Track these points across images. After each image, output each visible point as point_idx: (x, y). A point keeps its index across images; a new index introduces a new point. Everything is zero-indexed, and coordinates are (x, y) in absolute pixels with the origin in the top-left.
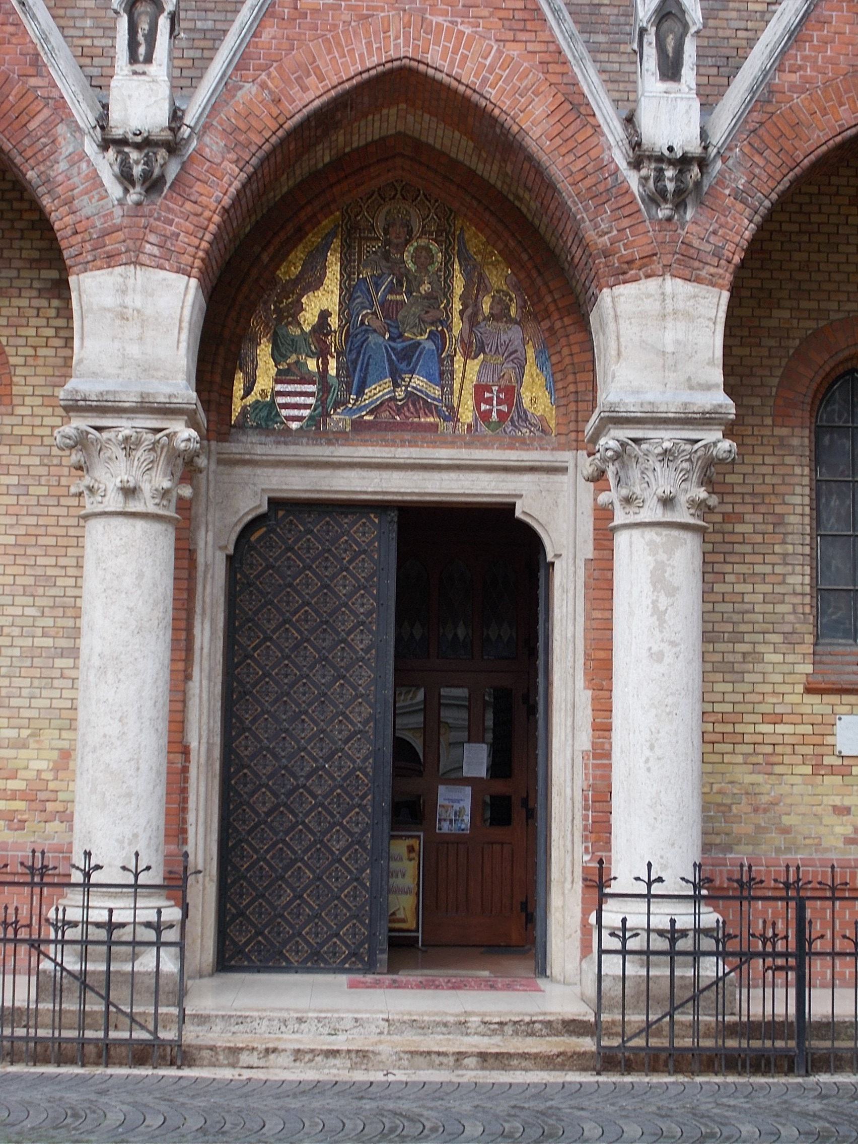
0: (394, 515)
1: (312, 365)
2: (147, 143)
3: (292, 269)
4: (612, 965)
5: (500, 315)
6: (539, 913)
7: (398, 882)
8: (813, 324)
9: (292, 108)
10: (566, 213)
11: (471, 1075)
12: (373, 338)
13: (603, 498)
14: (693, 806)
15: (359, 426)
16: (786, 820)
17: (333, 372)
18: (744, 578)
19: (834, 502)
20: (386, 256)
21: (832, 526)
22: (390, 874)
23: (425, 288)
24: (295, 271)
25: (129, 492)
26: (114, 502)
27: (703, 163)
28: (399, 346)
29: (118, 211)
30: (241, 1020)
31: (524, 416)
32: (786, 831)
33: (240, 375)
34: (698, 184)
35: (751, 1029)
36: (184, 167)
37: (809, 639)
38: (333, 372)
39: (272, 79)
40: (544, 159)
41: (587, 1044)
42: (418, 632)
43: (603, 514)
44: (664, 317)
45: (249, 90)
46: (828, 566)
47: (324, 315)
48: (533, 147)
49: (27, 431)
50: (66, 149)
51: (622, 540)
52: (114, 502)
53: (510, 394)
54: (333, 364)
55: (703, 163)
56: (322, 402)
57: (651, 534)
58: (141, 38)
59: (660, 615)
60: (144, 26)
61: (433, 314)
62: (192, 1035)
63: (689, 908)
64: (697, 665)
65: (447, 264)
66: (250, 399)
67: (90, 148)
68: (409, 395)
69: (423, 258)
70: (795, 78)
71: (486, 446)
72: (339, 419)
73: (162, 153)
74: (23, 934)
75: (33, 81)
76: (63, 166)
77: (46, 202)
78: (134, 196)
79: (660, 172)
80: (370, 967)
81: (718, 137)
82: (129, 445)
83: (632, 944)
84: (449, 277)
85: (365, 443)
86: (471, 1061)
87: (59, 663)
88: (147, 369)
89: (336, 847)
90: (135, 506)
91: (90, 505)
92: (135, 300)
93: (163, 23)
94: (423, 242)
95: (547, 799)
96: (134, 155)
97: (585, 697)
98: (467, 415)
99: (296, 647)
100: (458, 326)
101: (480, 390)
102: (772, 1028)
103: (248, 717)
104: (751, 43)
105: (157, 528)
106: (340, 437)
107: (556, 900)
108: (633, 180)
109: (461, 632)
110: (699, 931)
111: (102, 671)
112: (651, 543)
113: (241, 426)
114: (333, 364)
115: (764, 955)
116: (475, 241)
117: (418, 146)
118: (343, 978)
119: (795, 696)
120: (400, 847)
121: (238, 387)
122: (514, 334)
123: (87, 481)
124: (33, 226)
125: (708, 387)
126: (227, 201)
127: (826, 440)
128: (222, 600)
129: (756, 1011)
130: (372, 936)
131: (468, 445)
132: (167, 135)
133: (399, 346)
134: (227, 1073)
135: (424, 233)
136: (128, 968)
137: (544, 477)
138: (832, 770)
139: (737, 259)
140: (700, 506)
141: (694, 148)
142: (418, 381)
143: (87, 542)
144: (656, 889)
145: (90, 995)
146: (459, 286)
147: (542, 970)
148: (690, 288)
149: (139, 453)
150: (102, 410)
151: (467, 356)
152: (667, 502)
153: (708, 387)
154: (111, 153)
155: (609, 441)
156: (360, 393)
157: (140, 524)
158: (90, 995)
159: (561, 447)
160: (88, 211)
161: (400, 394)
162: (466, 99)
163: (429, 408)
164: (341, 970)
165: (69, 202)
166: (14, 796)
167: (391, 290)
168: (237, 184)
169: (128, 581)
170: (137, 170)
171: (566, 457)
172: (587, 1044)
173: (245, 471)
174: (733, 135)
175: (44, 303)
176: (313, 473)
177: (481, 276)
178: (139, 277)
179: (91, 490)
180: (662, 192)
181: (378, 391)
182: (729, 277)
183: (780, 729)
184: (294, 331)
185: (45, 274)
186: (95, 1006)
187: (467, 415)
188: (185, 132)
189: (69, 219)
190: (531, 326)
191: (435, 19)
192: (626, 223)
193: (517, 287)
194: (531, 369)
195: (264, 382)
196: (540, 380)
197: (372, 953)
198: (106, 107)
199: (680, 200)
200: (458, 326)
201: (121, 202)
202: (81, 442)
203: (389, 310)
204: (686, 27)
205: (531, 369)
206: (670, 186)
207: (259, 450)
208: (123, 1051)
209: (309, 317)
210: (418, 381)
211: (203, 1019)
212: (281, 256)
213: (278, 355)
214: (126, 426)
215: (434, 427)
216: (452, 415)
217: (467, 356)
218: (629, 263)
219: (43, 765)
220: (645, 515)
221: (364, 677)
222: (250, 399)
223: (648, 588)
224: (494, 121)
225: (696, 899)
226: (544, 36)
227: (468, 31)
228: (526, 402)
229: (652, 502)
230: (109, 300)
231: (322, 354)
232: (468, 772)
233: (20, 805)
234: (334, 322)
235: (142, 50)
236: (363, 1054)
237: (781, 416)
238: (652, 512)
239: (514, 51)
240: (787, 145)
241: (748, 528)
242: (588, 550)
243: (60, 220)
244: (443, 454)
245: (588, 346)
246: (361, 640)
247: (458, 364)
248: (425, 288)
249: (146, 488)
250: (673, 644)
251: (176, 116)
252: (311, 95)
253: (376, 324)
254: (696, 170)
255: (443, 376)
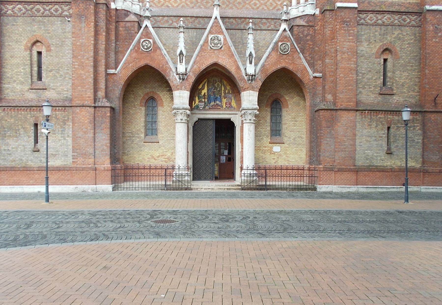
0: (215, 120)
1: (203, 100)
2: (183, 74)
3: (200, 87)
4: (243, 178)
5: (229, 93)
6: (234, 159)
7: (215, 169)
8: (271, 94)
9: (201, 69)
10: (237, 82)
11: (226, 191)
12: (211, 96)
13: (242, 119)
14: (253, 158)
15: (210, 108)
16: (267, 160)
17: (206, 101)
18: (261, 128)
19: (274, 118)
20: (213, 85)
21: (273, 121)
22: (215, 168)
23: (218, 89)
24: (201, 87)
25: (181, 120)
26: (180, 121)
27: (255, 76)
28: (215, 97)
29: (179, 83)
30: (198, 185)
31: (232, 107)
32: (266, 161)
33: (194, 102)
34: (254, 78)
35: (260, 185)
36: (187, 77)
37: (270, 136)
38: (206, 101)
39: (198, 65)
40: (234, 75)
41: (240, 187)
42: (217, 135)
43: (242, 121)
44: (250, 96)
45: (195, 66)
46: (273, 126)
47: (205, 93)
48: (233, 73)
49: (166, 110)
50: (172, 75)
51: (244, 124)
52: (180, 121)
53: (230, 104)
54: (206, 100)
55: (255, 76)
56: (205, 105)
57: (248, 124)
58: (181, 59)
59: (249, 134)
60: (181, 58)
61: (219, 93)
62: (192, 187)
63: (252, 171)
64: (254, 140)
65: (221, 86)
66: (195, 105)
67: (175, 74)
68: (216, 104)
69: (218, 85)
70: (267, 63)
71: (227, 111)
72: (207, 107)
73: (185, 75)
74: (172, 175)
75: (167, 65)
76: (171, 77)
77: (169, 82)
78: (181, 81)
79: (249, 77)
80: (212, 180)
81: (257, 72)
82: (181, 114)
83: (245, 175)
84: (222, 87)
85: (211, 111)
86: (226, 189)
87: (171, 141)
88: (183, 104)
89: (208, 164)
90: (182, 121)
91: (176, 121)
92: (181, 95)
93: (184, 57)
94: (218, 83)
95: (234, 174)
96: (181, 76)
97: (240, 144)
98: (224, 107)
99: (202, 138)
100: (223, 94)
101: (226, 103)
102: (262, 185)
103: (196, 148)
104: (263, 56)
105: (185, 124)
106: (207, 110)
107: (237, 171)
108: (246, 78)
109: (224, 135)
110: (253, 174)
111: (179, 142)
112: (248, 125)
113: (194, 109)
114: (206, 100)
115: (261, 176)
116: (225, 83)
117: (217, 70)
118: (209, 181)
119: (268, 144)
120: (216, 165)
121: (193, 103)
122: (231, 95)
123: (176, 118)
124: (165, 82)
125: (255, 105)
126: (193, 81)
127: (273, 109)
128: (192, 132)
129: (260, 184)
130: (212, 176)
131: (225, 111)
132: (185, 73)
133: (215, 97)
134: (197, 191)
135: (218, 82)
136: (184, 179)
137: (235, 115)
138: (273, 154)
139: (259, 88)
140: (254, 120)
141: (254, 74)
142: (218, 102)
143: (176, 126)
144: (248, 168)
145: (180, 182)
146: (223, 89)
147: (235, 180)
148: (253, 92)
149: (183, 114)
150: (178, 109)
151: (224, 99)
152: (250, 120)
153: (255, 105)
154: (178, 75)
155: (243, 112)
156: (210, 104)
157: (183, 124)
158: (180, 182)
159: (237, 111)
160: (175, 83)
161: (215, 104)
162: (224, 67)
163: (219, 106)
164: (208, 180)
165: (172, 82)
166: (166, 158)
167: (214, 90)
168: (194, 79)
169: (182, 131)
170: (181, 78)
171: (237, 112)
172: (240, 187)
173: (195, 115)
174: (259, 71)
175: (167, 93)
176: (204, 115)
177: (226, 88)
178: (182, 92)
179: (176, 119)
180: (250, 79)
181: (212, 103)
182: (258, 90)
183: (266, 148)
184: (201, 95)
185: (167, 89)
186: (180, 184)
187: (224, 107)
188: (187, 72)
189: (173, 84)
190: (233, 94)
191: (220, 56)
192: (245, 83)
193: (231, 89)
194: (233, 100)
195: (197, 103)
196: (234, 102)
197: (213, 178)
198: (177, 68)
199: (252, 80)
200: (223, 94)
201: (179, 82)
202: (175, 113)
203: (214, 92)
204: (253, 57)
205: (233, 100)
206: (251, 79)
207: (196, 112)
208: (184, 189)
209: (203, 94)
210: (218, 102)
211: (193, 185)
212: (199, 85)
213: (199, 99)
214: (181, 111)
215: (220, 108)
216: (222, 107)
217: (224, 99)
218: (245, 89)
219: (169, 154)
220: (247, 122)
221: (211, 142)
222: (195, 105)
223: (248, 131)
224: (228, 70)
225: (253, 169)
226: (234, 58)
227: (224, 58)
228: (232, 105)
229: (248, 120)
230: (178, 95)
231: (205, 99)
232: (225, 154)
233: (167, 160)
234: (206, 94)
235: (181, 61)
236: (213, 189)
237: (266, 107)
238: (248, 121)
239: (230, 60)
240: (266, 72)
241: (262, 122)
242: (241, 125)
243: (171, 84)
244: (221, 112)
245: (240, 100)
246: (210, 137)
247: (223, 100)
248: (218, 89)
249: (184, 119)
250: (251, 138)
251: (186, 70)
252: (204, 67)
253: (212, 94)
254: (254, 76)
255: (221, 101)
